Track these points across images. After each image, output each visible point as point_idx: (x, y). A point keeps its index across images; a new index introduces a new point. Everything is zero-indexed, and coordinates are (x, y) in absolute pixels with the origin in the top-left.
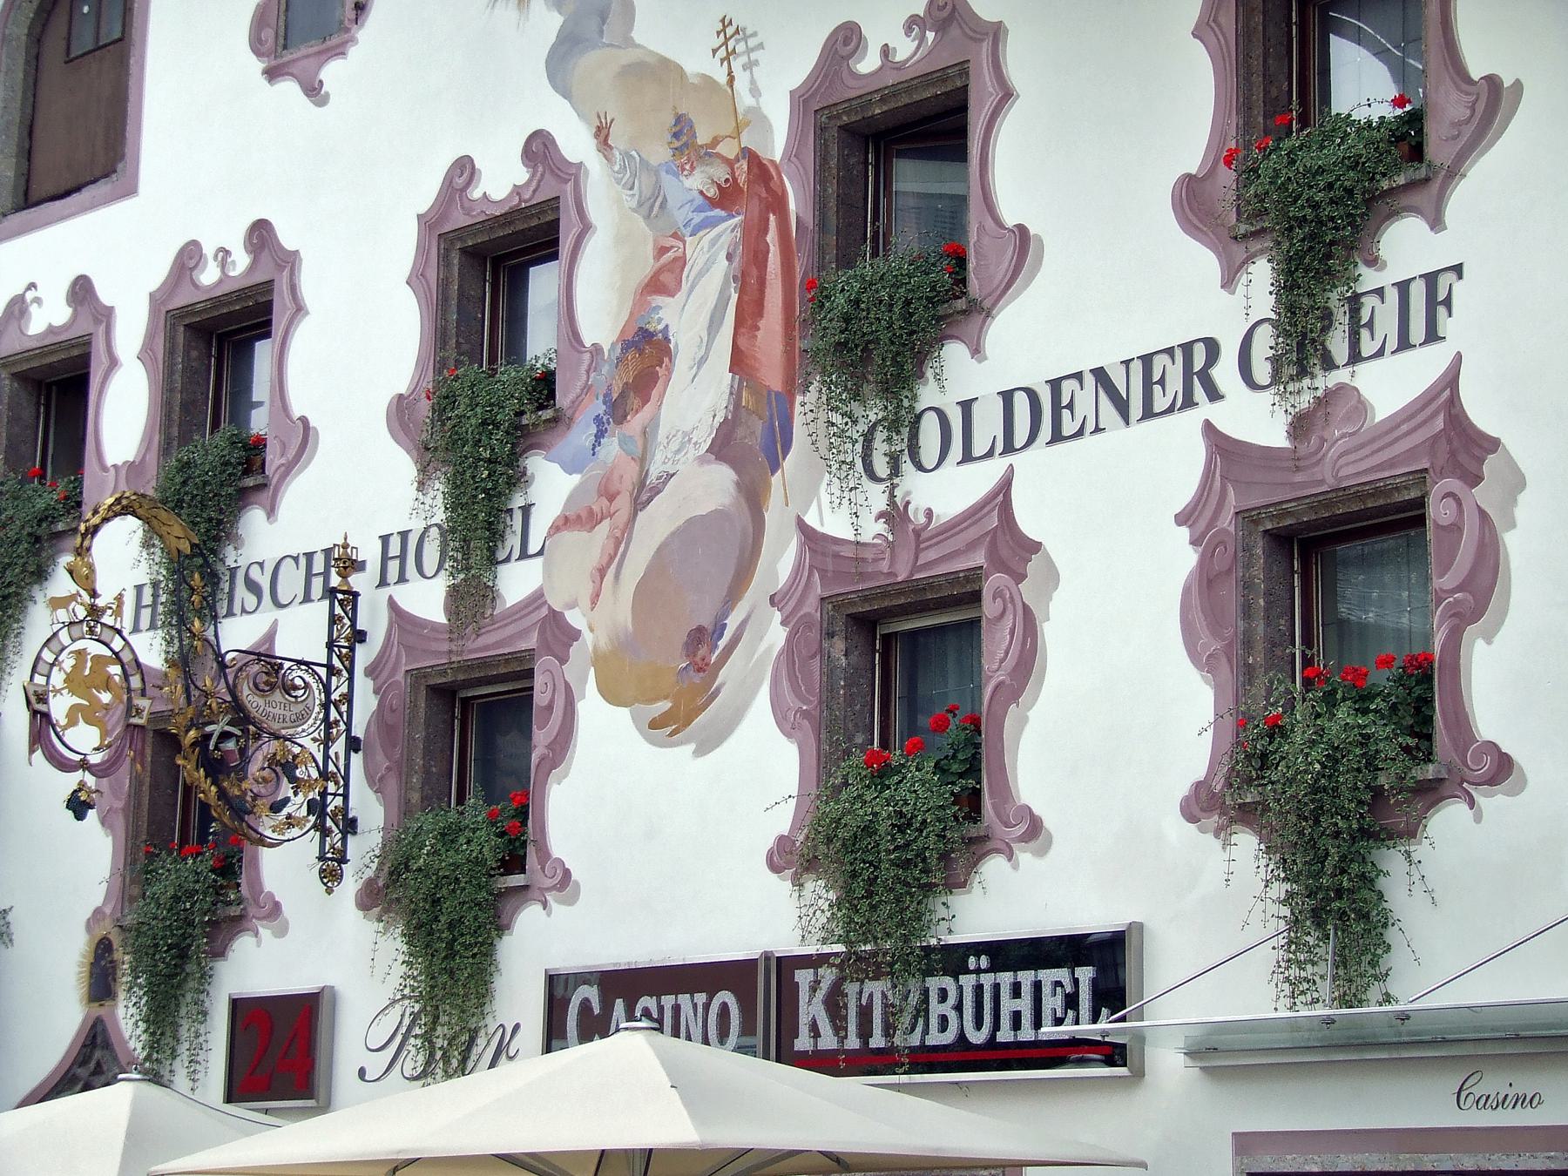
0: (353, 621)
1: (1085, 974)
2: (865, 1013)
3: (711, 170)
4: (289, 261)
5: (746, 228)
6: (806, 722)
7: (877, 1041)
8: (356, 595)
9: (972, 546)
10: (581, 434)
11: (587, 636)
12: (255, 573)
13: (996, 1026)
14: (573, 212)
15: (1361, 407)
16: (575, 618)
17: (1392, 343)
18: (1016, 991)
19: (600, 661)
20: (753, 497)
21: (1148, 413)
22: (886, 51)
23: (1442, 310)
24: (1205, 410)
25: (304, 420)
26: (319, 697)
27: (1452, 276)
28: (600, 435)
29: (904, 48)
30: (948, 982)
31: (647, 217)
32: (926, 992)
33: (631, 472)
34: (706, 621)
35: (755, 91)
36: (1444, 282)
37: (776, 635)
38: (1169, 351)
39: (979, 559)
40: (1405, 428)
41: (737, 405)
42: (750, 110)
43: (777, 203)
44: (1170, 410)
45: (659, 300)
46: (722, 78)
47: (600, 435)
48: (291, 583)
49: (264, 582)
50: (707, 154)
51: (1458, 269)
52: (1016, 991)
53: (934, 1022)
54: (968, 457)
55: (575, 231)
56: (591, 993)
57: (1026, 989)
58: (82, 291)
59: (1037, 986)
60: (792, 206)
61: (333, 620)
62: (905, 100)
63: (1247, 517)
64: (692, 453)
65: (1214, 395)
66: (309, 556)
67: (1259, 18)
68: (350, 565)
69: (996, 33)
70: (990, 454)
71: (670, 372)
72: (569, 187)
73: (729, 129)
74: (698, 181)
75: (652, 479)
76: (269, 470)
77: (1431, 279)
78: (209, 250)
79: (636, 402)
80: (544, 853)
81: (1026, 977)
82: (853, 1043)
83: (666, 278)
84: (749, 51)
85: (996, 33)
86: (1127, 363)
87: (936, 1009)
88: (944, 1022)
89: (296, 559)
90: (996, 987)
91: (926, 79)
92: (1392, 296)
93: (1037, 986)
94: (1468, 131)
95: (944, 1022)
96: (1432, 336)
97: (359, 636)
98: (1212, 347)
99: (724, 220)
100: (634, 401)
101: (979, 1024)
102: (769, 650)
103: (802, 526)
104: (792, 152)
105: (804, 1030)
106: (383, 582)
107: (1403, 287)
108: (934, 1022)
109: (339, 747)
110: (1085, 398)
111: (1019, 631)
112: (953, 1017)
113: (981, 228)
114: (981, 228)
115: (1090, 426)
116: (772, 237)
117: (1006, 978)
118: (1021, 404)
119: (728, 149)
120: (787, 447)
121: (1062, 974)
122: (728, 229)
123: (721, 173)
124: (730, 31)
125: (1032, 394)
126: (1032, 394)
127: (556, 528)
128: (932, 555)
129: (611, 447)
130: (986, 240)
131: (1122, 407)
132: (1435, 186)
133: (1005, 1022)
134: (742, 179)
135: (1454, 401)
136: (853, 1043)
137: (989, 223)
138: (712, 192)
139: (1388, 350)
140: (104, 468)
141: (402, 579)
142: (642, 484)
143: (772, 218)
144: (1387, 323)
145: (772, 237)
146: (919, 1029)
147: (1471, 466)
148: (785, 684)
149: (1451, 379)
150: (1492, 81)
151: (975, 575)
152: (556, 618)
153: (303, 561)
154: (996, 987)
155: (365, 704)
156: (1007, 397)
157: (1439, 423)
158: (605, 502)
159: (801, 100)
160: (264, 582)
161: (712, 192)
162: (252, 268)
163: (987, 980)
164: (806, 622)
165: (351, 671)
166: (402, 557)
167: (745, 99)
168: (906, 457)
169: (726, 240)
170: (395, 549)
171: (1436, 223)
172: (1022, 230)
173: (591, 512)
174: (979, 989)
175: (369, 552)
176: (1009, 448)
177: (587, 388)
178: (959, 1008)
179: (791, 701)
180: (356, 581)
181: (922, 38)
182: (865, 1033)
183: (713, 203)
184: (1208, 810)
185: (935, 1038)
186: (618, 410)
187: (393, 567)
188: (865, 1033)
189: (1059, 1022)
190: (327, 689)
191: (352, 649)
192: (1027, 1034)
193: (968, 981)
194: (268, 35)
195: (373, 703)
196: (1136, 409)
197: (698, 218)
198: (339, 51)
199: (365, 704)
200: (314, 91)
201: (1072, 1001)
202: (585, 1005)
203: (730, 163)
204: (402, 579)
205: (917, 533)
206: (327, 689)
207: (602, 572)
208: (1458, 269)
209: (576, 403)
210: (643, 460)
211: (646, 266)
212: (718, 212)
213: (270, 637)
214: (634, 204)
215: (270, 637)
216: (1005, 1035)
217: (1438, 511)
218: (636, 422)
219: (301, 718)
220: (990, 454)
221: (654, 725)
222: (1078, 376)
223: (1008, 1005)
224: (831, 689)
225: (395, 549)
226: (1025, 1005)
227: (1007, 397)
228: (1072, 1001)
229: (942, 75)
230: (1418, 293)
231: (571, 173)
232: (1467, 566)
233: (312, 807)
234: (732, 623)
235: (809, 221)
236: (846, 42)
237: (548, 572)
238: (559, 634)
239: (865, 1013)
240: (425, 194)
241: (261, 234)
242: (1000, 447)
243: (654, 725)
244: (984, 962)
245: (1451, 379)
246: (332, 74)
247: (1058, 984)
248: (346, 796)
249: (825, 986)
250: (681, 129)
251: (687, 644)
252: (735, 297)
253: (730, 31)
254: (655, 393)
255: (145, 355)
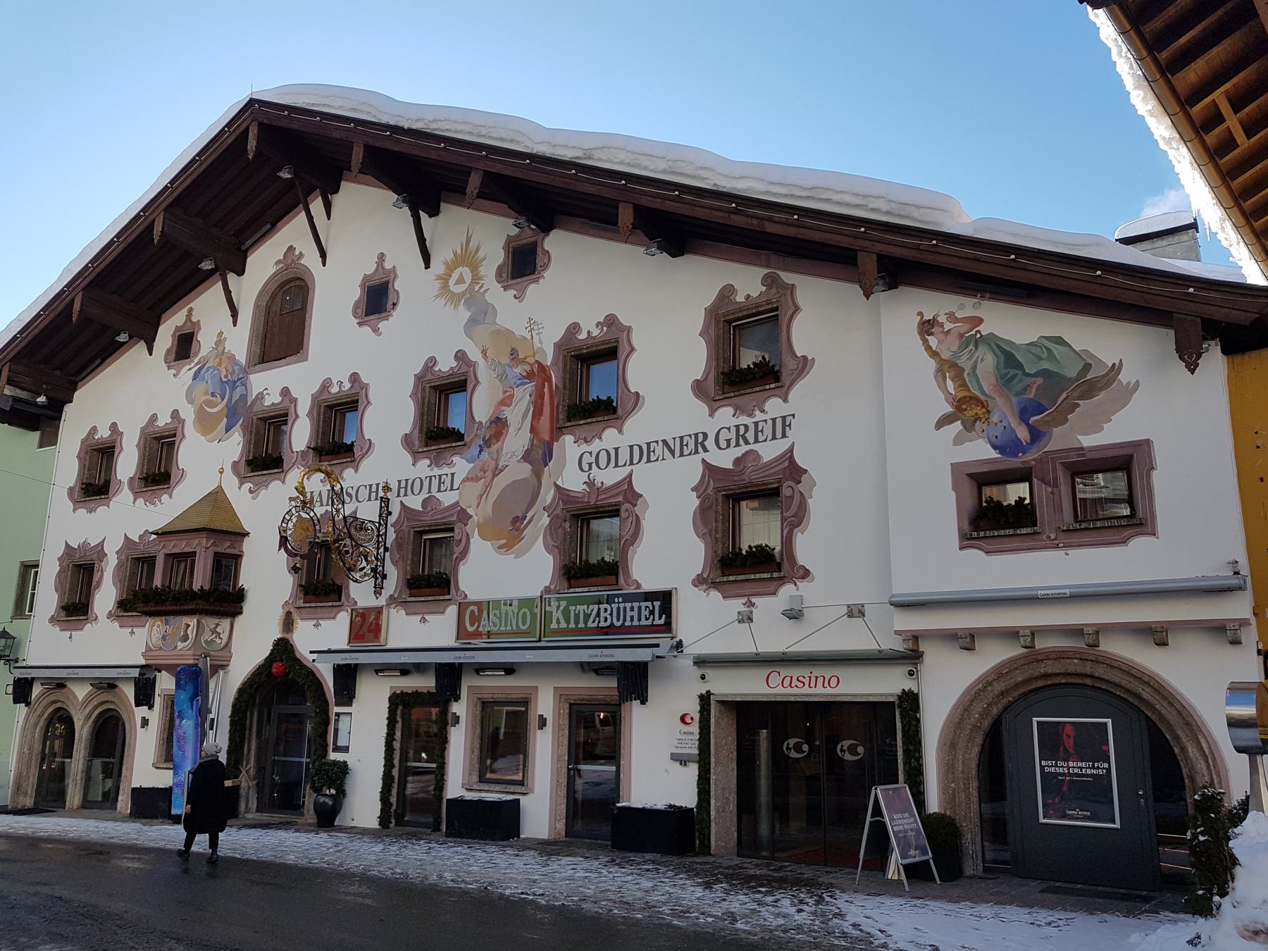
0: (388, 508)
1: (657, 604)
2: (577, 616)
3: (524, 367)
4: (365, 387)
5: (536, 386)
6: (556, 550)
7: (581, 625)
8: (389, 499)
9: (617, 494)
10: (474, 450)
11: (475, 517)
12: (350, 490)
13: (625, 620)
14: (473, 378)
15: (759, 457)
16: (470, 511)
17: (770, 437)
18: (632, 609)
19: (480, 526)
20: (538, 475)
21: (682, 455)
22: (589, 332)
23: (787, 428)
24: (702, 455)
25: (370, 440)
26: (376, 533)
27: (792, 417)
28: (481, 451)
29: (595, 332)
30: (607, 606)
31: (500, 381)
32: (599, 609)
33: (493, 464)
34: (520, 515)
35: (541, 342)
36: (788, 419)
37: (546, 520)
38: (690, 436)
39: (620, 499)
40: (774, 465)
41: (532, 444)
42: (538, 348)
43: (549, 379)
44: (690, 454)
45: (503, 408)
46: (529, 338)
47: (481, 451)
48: (364, 494)
49: (354, 494)
50: (523, 361)
51: (793, 415)
52: (632, 609)
53: (602, 619)
54: (616, 465)
55: (473, 383)
56: (475, 608)
57: (636, 609)
58: (285, 392)
59: (640, 608)
60: (554, 380)
61: (381, 507)
62: (594, 349)
63: (717, 490)
64: (515, 459)
65: (706, 450)
66: (371, 486)
67: (721, 331)
68: (387, 488)
69: (629, 329)
70: (625, 465)
71: (507, 432)
72: (471, 369)
73: (531, 354)
74: (519, 370)
75: (500, 467)
76: (356, 456)
77: (784, 418)
78: (335, 381)
79: (495, 442)
80: (457, 588)
81: (636, 605)
82: (572, 625)
83: (507, 401)
84: (539, 329)
85: (629, 329)
86: (674, 438)
87: (603, 615)
88: (606, 619)
89: (366, 486)
90: (625, 608)
91: (604, 343)
92: (770, 422)
93: (640, 608)
94: (796, 372)
95: (606, 619)
96: (784, 436)
97: (390, 513)
98: (705, 436)
99: (527, 383)
100: (494, 440)
101: (618, 620)
102: (543, 525)
103: (555, 484)
104: (554, 362)
105: (554, 621)
106: (398, 496)
107: (774, 420)
108: (602, 619)
109: (382, 550)
110: (659, 449)
111: (634, 522)
112: (609, 617)
113: (623, 392)
114: (623, 392)
115: (661, 458)
116: (546, 390)
117: (628, 605)
118: (636, 449)
119: (531, 360)
120: (550, 459)
121: (649, 604)
122: (530, 387)
123: (528, 368)
124: (532, 322)
125: (640, 447)
126: (640, 447)
127: (463, 481)
128: (603, 497)
129: (485, 455)
130: (624, 396)
131: (672, 452)
132: (785, 389)
133: (628, 618)
134: (535, 371)
135: (792, 457)
136: (572, 625)
137: (626, 390)
138: (524, 374)
139: (768, 439)
140: (293, 452)
141: (406, 495)
142: (497, 468)
143: (546, 384)
144: (768, 431)
145: (546, 390)
146: (596, 622)
147: (798, 478)
148: (549, 536)
149: (791, 450)
150: (805, 358)
151: (618, 504)
152: (463, 510)
153: (368, 487)
154: (625, 608)
155: (391, 536)
156: (631, 447)
157: (786, 464)
158: (482, 473)
159: (558, 346)
160: (354, 494)
161: (524, 374)
162: (350, 388)
163: (622, 606)
164: (557, 516)
165: (386, 525)
166: (406, 488)
167: (537, 345)
168: (594, 465)
169: (530, 389)
170: (403, 484)
171: (785, 400)
172: (637, 393)
173: (477, 476)
174: (619, 609)
175: (394, 485)
176: (631, 463)
177: (476, 435)
178: (611, 614)
179: (551, 542)
180: (389, 495)
181: (602, 329)
182: (577, 622)
183: (525, 377)
184: (702, 584)
185: (602, 624)
186: (487, 443)
187: (402, 491)
188: (577, 622)
189: (647, 619)
190: (379, 530)
191: (387, 517)
192: (636, 623)
193: (615, 606)
194: (359, 311)
195: (394, 536)
196: (677, 453)
197: (519, 382)
198: (386, 318)
199: (391, 536)
200: (376, 330)
201: (652, 612)
202: (472, 612)
203: (531, 365)
204: (406, 495)
205: (598, 489)
206: (379, 530)
207: (481, 496)
208: (793, 415)
209: (472, 441)
210: (497, 460)
211: (500, 396)
212: (526, 381)
213: (355, 512)
214: (495, 376)
215: (355, 512)
216: (628, 623)
217: (786, 491)
218: (494, 448)
219: (370, 540)
220: (625, 465)
221: (499, 548)
222: (657, 442)
223: (629, 613)
224: (565, 539)
225: (403, 484)
226: (635, 613)
227: (631, 447)
228: (652, 612)
229: (609, 342)
230: (779, 422)
231: (473, 365)
232: (796, 508)
233: (372, 570)
234: (529, 516)
235: (560, 385)
236: (574, 329)
237: (460, 494)
238: (464, 516)
239: (577, 616)
240: (418, 369)
241: (355, 378)
242: (628, 463)
243: (499, 548)
244: (621, 600)
245: (791, 450)
246: (382, 325)
247: (647, 607)
248: (383, 567)
249: (562, 608)
250: (513, 353)
251: (512, 522)
252: (532, 409)
253: (532, 322)
254: (502, 439)
255: (310, 414)
